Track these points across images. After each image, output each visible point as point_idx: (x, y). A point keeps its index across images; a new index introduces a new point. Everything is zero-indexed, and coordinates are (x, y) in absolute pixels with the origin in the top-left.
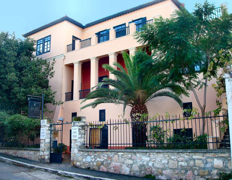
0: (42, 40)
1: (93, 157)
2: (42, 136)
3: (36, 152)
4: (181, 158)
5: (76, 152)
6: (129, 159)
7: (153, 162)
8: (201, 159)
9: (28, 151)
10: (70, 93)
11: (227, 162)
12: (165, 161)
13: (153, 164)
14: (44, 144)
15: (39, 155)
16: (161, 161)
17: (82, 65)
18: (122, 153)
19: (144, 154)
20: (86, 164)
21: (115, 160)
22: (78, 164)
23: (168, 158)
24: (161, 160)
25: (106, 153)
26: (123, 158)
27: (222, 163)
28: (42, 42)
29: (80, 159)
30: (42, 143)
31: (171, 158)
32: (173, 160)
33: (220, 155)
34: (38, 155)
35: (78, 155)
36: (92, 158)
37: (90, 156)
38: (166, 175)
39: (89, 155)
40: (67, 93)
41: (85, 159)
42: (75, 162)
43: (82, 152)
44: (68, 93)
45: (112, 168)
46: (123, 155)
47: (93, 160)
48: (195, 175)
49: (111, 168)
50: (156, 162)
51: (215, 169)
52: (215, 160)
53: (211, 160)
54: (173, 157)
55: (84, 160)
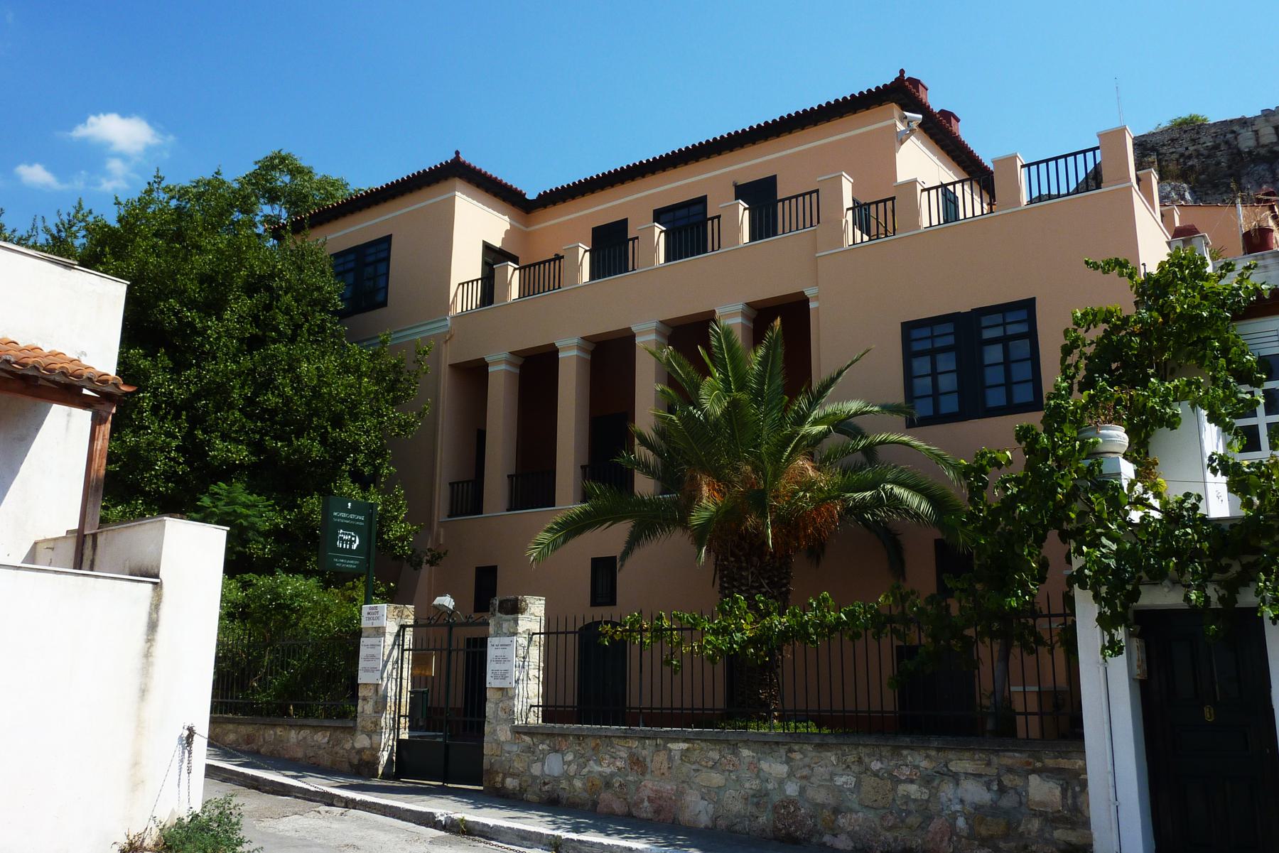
0: (352, 257)
1: (570, 757)
2: (366, 670)
3: (339, 734)
4: (906, 771)
5: (503, 739)
6: (712, 768)
7: (804, 782)
8: (980, 776)
9: (304, 733)
10: (468, 482)
11: (1077, 789)
12: (844, 779)
13: (802, 790)
14: (371, 703)
15: (353, 747)
16: (831, 779)
17: (522, 367)
18: (684, 746)
19: (767, 748)
20: (545, 784)
21: (657, 773)
22: (511, 783)
23: (855, 768)
24: (832, 775)
25: (622, 742)
26: (689, 762)
27: (1058, 792)
28: (352, 265)
29: (518, 766)
30: (365, 699)
31: (867, 769)
32: (876, 774)
33: (1050, 763)
34: (348, 746)
35: (515, 748)
36: (569, 763)
37: (559, 755)
38: (852, 835)
39: (557, 751)
40: (458, 483)
41: (539, 764)
42: (499, 779)
43: (527, 739)
44: (463, 482)
45: (646, 804)
46: (688, 749)
47: (573, 768)
48: (957, 835)
49: (642, 801)
50: (813, 779)
51: (1035, 815)
52: (1034, 780)
53: (1018, 781)
54: (876, 765)
55: (536, 769)
